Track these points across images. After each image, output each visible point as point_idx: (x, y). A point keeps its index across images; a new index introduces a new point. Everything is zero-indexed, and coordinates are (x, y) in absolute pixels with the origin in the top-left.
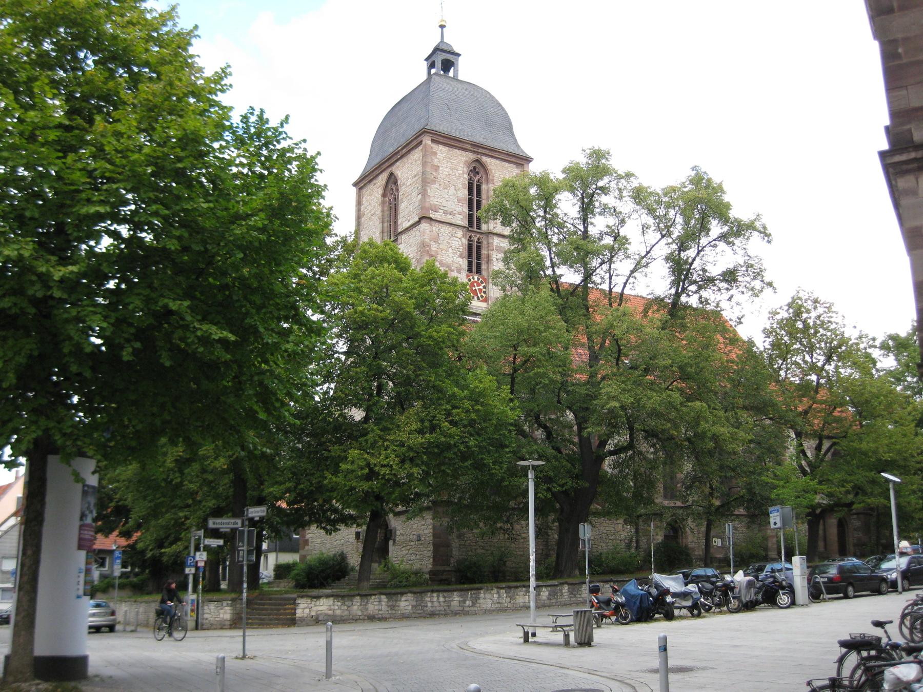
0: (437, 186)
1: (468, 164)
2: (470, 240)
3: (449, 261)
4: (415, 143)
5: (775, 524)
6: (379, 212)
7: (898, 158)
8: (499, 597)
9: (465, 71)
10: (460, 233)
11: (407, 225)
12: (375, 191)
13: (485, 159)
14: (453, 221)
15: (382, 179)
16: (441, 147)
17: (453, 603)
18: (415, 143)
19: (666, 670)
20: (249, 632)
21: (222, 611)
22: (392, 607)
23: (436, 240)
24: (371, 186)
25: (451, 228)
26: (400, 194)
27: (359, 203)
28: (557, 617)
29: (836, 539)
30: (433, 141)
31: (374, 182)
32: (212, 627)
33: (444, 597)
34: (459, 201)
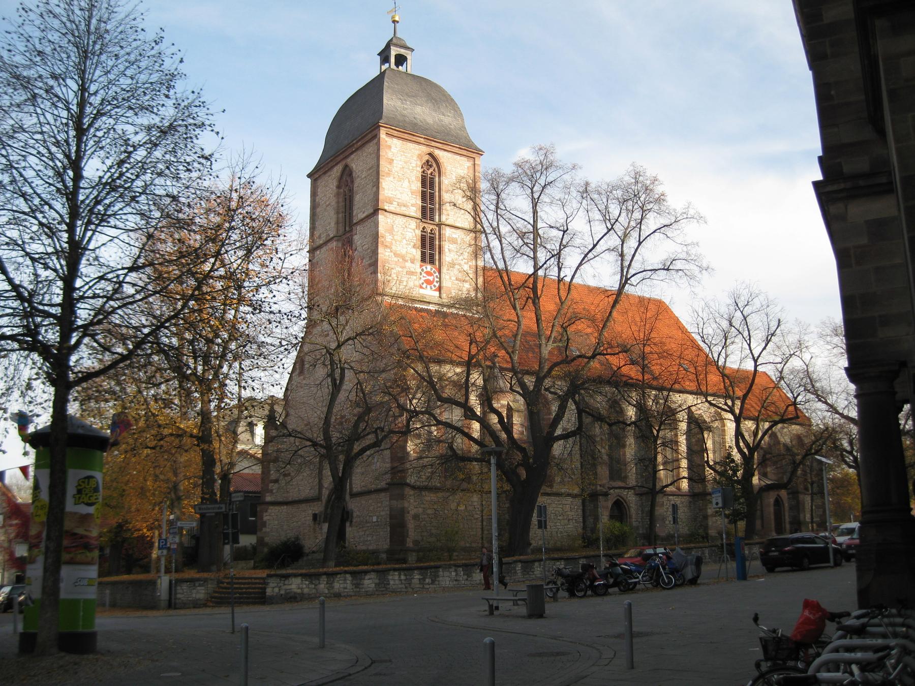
0: (391, 178)
1: (420, 157)
3: (404, 252)
4: (370, 136)
5: (717, 504)
6: (333, 203)
7: (830, 188)
10: (413, 224)
11: (361, 216)
12: (330, 183)
14: (407, 213)
15: (337, 170)
16: (395, 140)
17: (413, 581)
18: (370, 136)
19: (632, 635)
20: (237, 610)
21: (194, 591)
22: (357, 585)
24: (326, 177)
26: (356, 185)
27: (314, 194)
28: (518, 591)
29: (772, 517)
31: (329, 173)
32: (184, 606)
33: (405, 575)
34: (412, 193)
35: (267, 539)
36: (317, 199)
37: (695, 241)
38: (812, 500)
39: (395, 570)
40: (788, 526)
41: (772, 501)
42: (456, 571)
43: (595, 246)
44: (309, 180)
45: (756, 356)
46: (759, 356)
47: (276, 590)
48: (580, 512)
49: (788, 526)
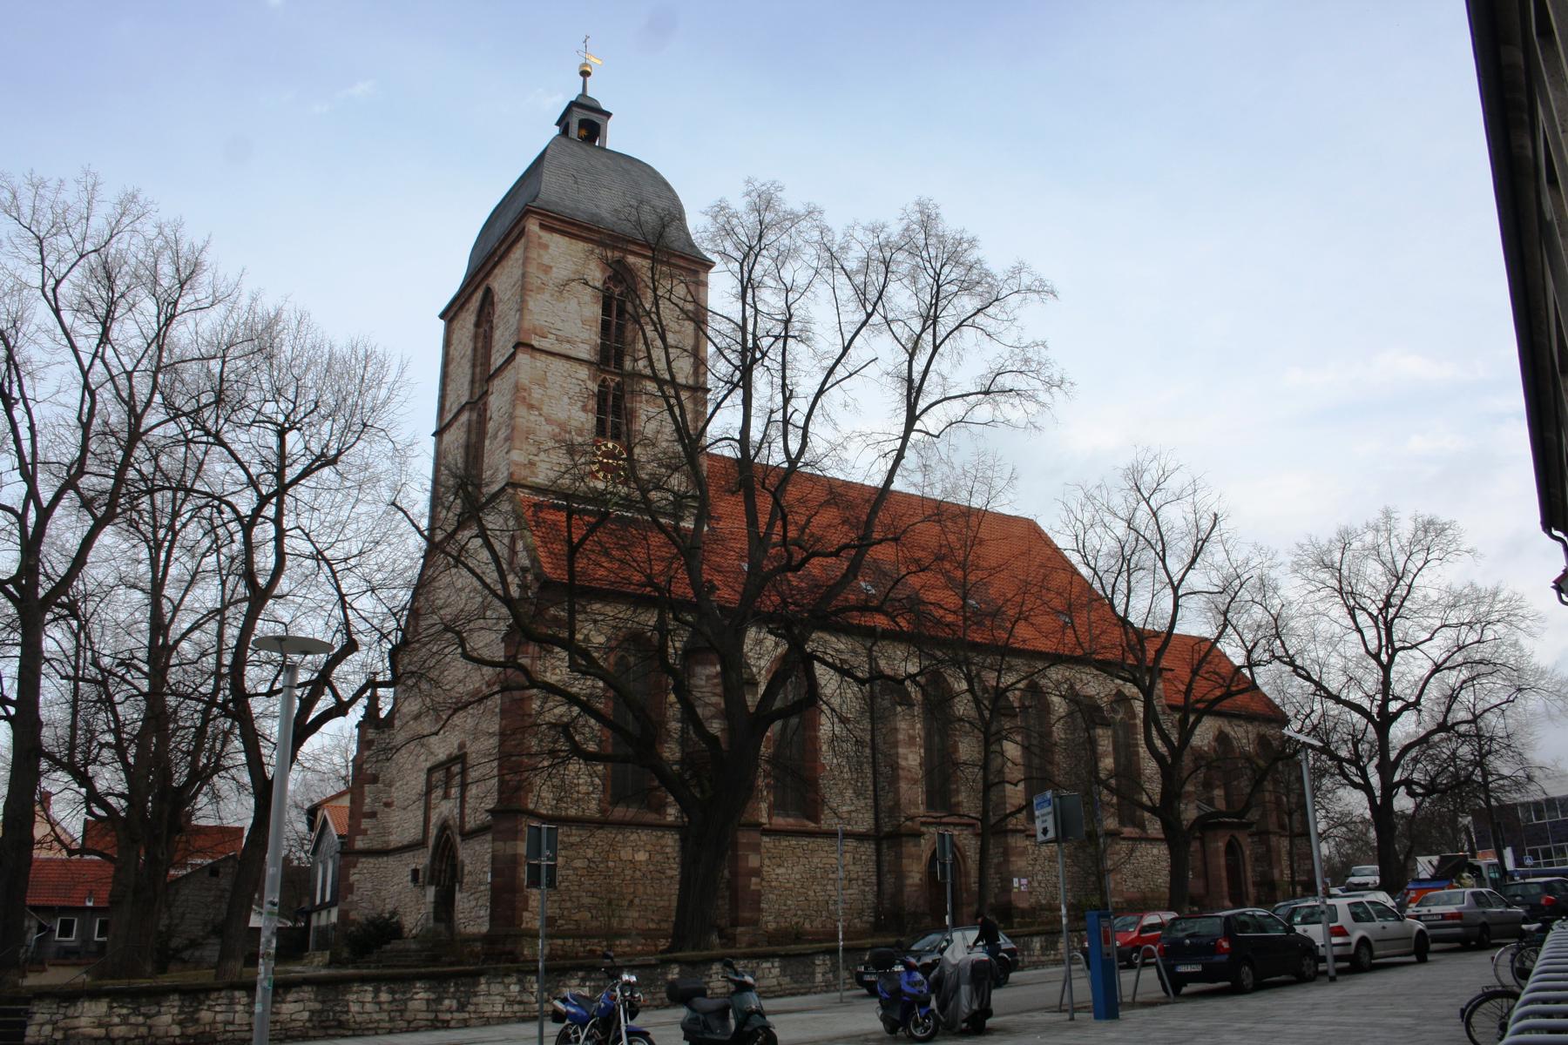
2: (603, 384)
3: (562, 416)
5: (1045, 831)
8: (523, 990)
9: (616, 138)
10: (583, 372)
12: (468, 318)
13: (1237, 834)
14: (573, 353)
16: (556, 237)
17: (411, 1005)
23: (542, 382)
25: (567, 365)
29: (1224, 874)
30: (542, 226)
33: (392, 992)
35: (353, 915)
36: (452, 351)
37: (1039, 339)
38: (1291, 843)
39: (364, 980)
40: (1252, 890)
41: (1221, 845)
42: (520, 982)
43: (846, 350)
44: (442, 323)
45: (1176, 580)
46: (1182, 580)
47: (48, 1029)
48: (872, 866)
49: (1252, 890)
